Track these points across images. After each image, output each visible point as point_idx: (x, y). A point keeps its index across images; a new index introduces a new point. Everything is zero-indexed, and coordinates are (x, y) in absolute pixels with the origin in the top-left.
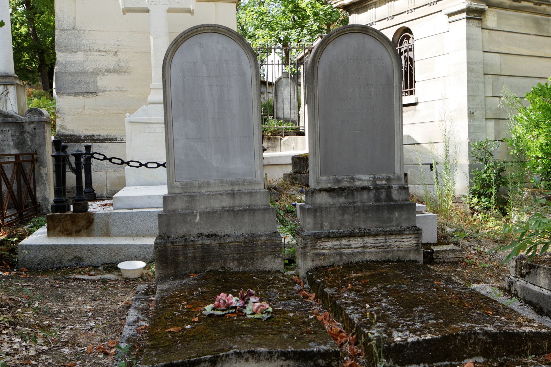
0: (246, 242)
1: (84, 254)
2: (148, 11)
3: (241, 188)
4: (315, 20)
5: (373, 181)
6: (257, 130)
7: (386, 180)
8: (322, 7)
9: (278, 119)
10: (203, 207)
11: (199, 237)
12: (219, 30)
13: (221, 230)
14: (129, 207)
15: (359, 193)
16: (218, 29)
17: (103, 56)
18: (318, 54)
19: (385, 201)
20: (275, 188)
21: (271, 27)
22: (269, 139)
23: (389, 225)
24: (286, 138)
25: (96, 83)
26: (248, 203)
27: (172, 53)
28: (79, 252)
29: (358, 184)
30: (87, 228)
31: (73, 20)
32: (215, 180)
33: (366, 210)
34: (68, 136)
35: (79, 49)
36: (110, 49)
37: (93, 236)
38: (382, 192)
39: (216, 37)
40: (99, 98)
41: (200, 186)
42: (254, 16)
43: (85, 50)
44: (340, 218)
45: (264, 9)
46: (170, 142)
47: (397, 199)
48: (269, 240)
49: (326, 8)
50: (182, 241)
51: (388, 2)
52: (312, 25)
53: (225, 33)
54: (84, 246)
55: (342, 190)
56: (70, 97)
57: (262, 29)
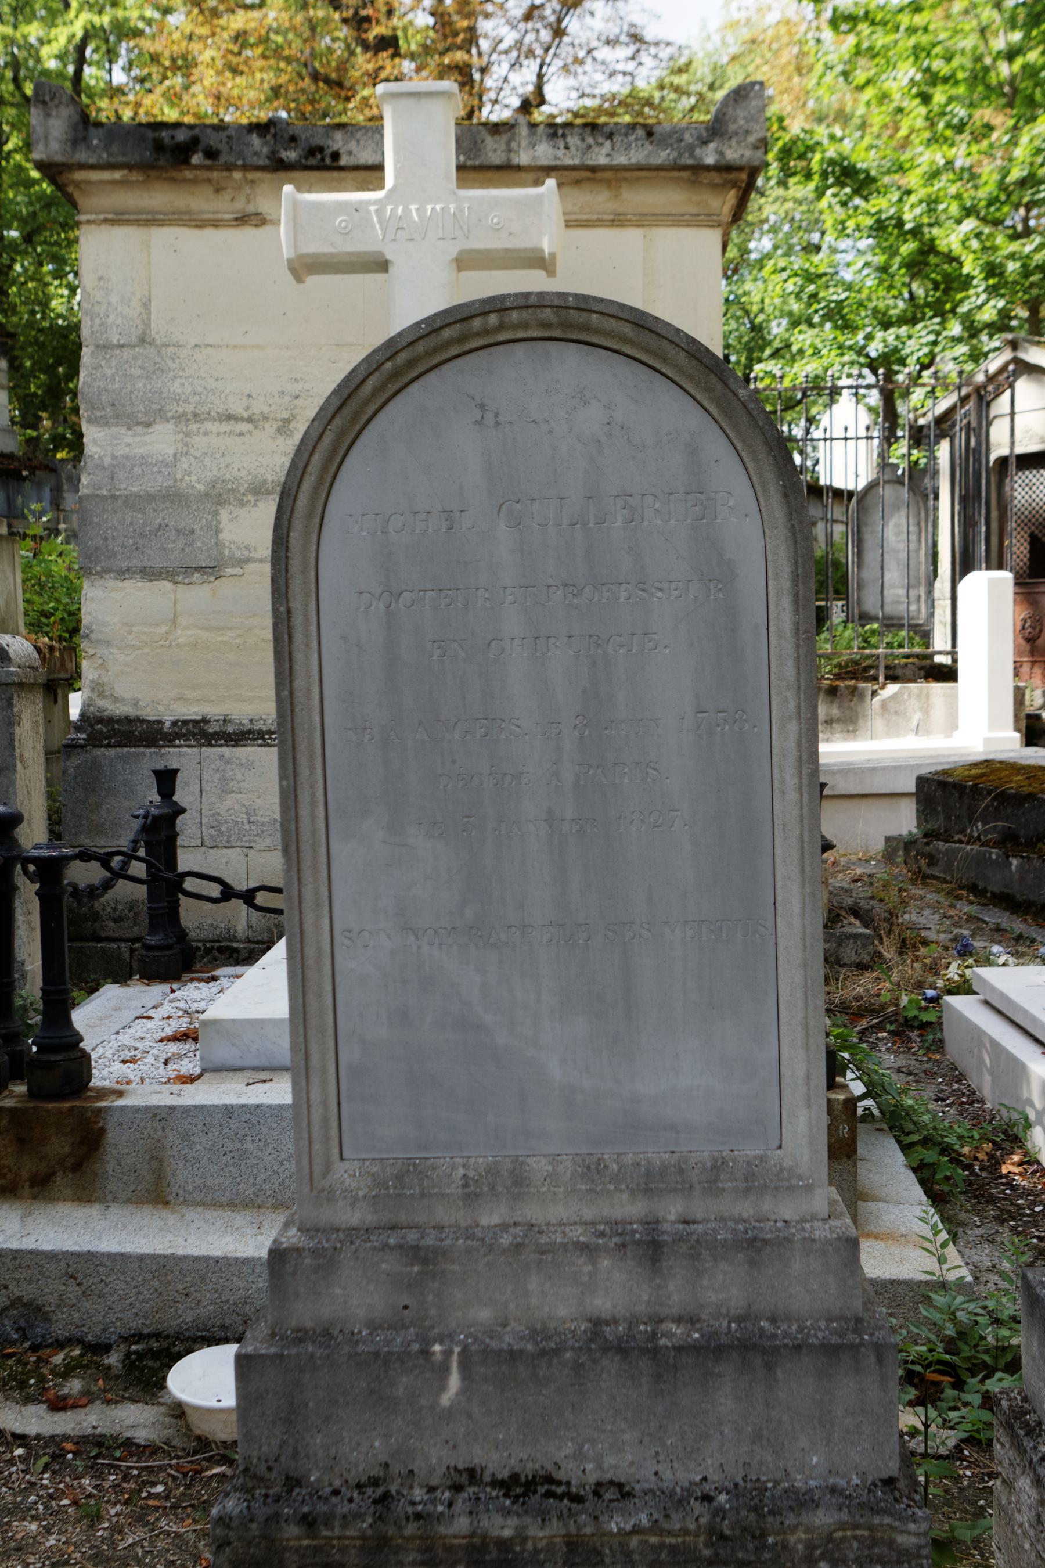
0: (722, 1537)
1: (49, 1291)
2: (382, 265)
3: (700, 1207)
4: (993, 291)
6: (795, 888)
8: (1014, 247)
9: (865, 618)
10: (484, 1314)
11: (457, 1488)
12: (587, 328)
13: (579, 1455)
14: (265, 1063)
16: (581, 317)
17: (241, 434)
20: (855, 911)
21: (843, 317)
22: (832, 692)
24: (892, 688)
25: (218, 531)
26: (736, 1298)
27: (328, 461)
28: (30, 1281)
30: (77, 1167)
31: (140, 309)
32: (554, 1159)
34: (119, 721)
35: (161, 414)
36: (266, 410)
37: (99, 1200)
39: (570, 366)
40: (224, 586)
41: (472, 1193)
42: (790, 287)
43: (180, 418)
45: (820, 261)
46: (310, 951)
48: (856, 1526)
49: (1028, 249)
50: (359, 1516)
52: (980, 307)
53: (624, 339)
54: (52, 1256)
56: (128, 584)
57: (811, 325)
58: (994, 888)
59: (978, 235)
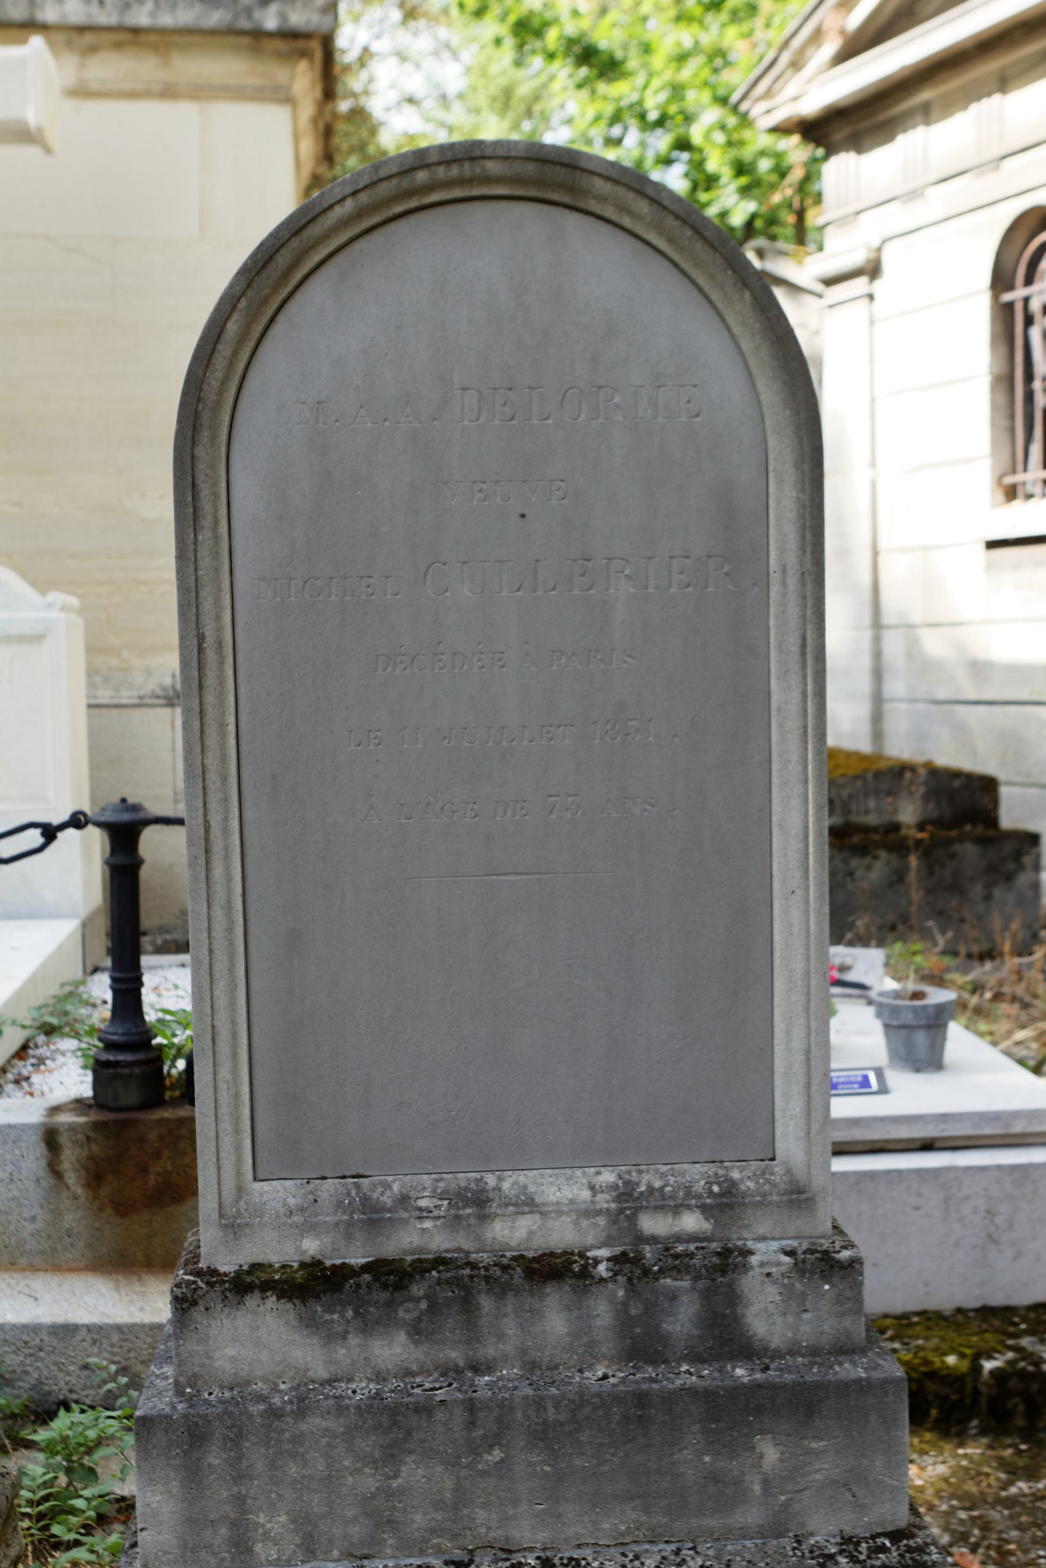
5: (615, 1217)
7: (704, 1209)
15: (511, 1302)
18: (225, 349)
19: (697, 1358)
23: (712, 1522)
29: (512, 1233)
33: (559, 1425)
38: (673, 1297)
44: (370, 1482)
47: (776, 1343)
51: (978, 99)
55: (392, 1276)
58: (215, 1023)
59: (723, 127)
